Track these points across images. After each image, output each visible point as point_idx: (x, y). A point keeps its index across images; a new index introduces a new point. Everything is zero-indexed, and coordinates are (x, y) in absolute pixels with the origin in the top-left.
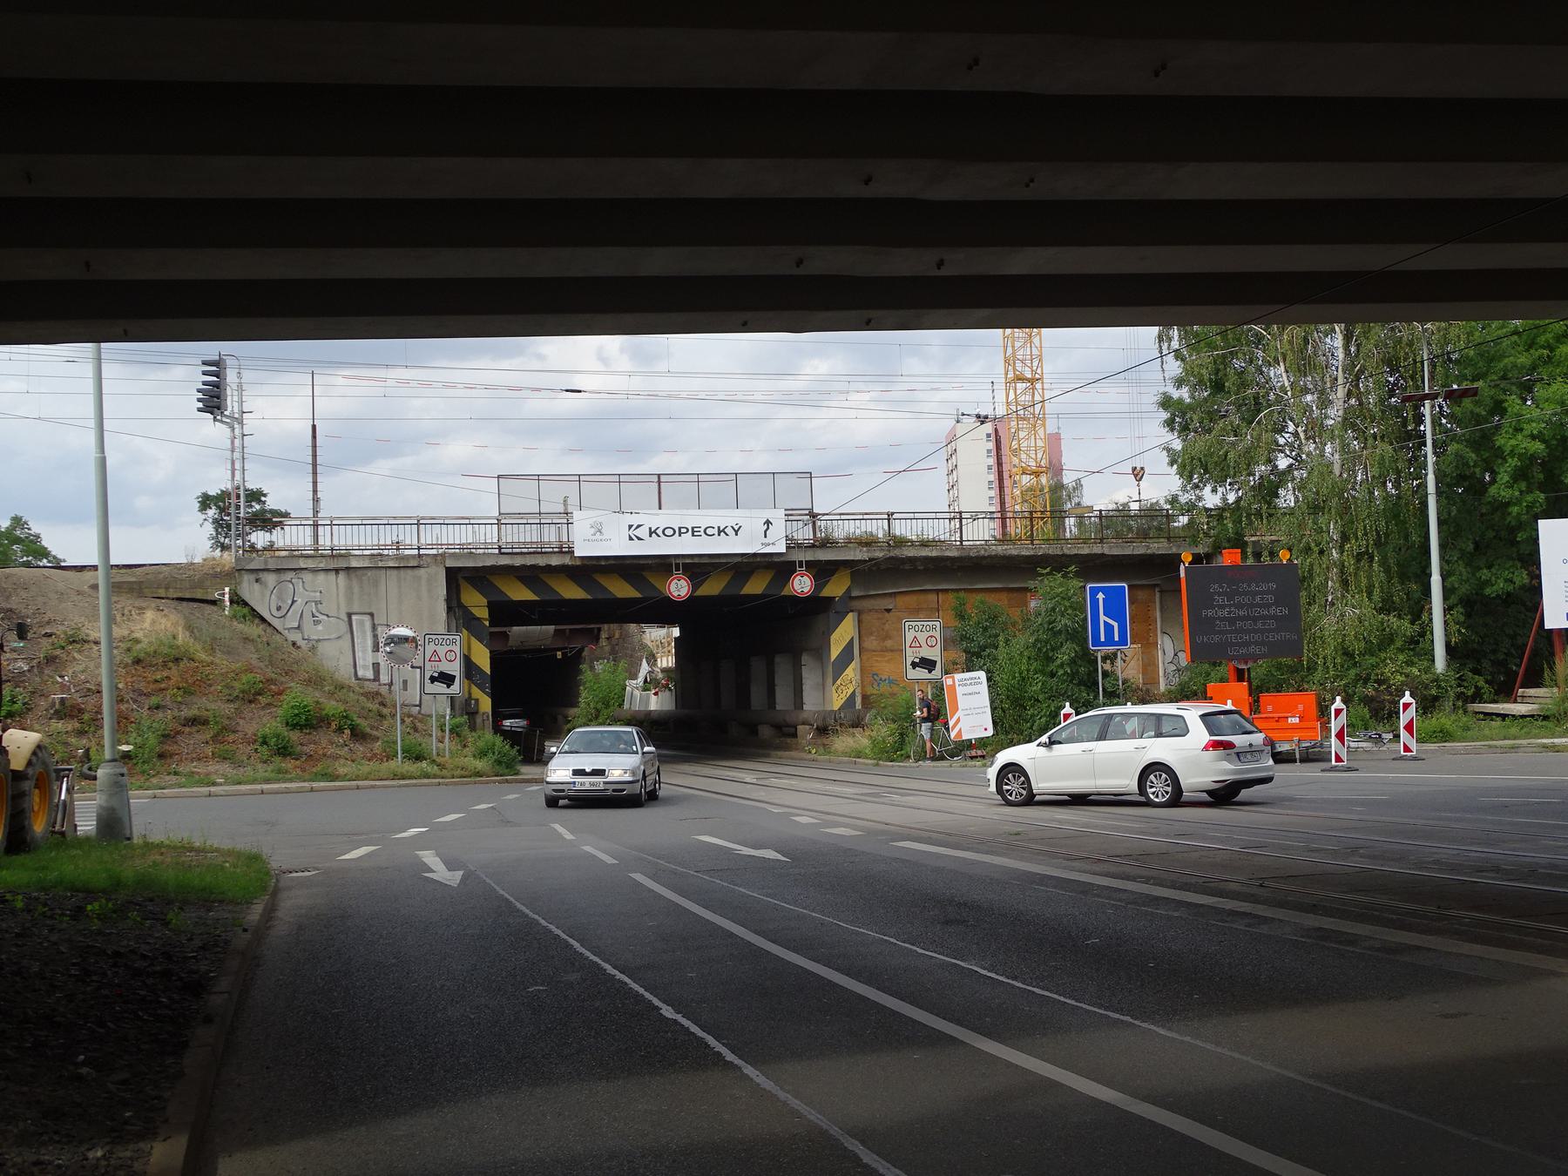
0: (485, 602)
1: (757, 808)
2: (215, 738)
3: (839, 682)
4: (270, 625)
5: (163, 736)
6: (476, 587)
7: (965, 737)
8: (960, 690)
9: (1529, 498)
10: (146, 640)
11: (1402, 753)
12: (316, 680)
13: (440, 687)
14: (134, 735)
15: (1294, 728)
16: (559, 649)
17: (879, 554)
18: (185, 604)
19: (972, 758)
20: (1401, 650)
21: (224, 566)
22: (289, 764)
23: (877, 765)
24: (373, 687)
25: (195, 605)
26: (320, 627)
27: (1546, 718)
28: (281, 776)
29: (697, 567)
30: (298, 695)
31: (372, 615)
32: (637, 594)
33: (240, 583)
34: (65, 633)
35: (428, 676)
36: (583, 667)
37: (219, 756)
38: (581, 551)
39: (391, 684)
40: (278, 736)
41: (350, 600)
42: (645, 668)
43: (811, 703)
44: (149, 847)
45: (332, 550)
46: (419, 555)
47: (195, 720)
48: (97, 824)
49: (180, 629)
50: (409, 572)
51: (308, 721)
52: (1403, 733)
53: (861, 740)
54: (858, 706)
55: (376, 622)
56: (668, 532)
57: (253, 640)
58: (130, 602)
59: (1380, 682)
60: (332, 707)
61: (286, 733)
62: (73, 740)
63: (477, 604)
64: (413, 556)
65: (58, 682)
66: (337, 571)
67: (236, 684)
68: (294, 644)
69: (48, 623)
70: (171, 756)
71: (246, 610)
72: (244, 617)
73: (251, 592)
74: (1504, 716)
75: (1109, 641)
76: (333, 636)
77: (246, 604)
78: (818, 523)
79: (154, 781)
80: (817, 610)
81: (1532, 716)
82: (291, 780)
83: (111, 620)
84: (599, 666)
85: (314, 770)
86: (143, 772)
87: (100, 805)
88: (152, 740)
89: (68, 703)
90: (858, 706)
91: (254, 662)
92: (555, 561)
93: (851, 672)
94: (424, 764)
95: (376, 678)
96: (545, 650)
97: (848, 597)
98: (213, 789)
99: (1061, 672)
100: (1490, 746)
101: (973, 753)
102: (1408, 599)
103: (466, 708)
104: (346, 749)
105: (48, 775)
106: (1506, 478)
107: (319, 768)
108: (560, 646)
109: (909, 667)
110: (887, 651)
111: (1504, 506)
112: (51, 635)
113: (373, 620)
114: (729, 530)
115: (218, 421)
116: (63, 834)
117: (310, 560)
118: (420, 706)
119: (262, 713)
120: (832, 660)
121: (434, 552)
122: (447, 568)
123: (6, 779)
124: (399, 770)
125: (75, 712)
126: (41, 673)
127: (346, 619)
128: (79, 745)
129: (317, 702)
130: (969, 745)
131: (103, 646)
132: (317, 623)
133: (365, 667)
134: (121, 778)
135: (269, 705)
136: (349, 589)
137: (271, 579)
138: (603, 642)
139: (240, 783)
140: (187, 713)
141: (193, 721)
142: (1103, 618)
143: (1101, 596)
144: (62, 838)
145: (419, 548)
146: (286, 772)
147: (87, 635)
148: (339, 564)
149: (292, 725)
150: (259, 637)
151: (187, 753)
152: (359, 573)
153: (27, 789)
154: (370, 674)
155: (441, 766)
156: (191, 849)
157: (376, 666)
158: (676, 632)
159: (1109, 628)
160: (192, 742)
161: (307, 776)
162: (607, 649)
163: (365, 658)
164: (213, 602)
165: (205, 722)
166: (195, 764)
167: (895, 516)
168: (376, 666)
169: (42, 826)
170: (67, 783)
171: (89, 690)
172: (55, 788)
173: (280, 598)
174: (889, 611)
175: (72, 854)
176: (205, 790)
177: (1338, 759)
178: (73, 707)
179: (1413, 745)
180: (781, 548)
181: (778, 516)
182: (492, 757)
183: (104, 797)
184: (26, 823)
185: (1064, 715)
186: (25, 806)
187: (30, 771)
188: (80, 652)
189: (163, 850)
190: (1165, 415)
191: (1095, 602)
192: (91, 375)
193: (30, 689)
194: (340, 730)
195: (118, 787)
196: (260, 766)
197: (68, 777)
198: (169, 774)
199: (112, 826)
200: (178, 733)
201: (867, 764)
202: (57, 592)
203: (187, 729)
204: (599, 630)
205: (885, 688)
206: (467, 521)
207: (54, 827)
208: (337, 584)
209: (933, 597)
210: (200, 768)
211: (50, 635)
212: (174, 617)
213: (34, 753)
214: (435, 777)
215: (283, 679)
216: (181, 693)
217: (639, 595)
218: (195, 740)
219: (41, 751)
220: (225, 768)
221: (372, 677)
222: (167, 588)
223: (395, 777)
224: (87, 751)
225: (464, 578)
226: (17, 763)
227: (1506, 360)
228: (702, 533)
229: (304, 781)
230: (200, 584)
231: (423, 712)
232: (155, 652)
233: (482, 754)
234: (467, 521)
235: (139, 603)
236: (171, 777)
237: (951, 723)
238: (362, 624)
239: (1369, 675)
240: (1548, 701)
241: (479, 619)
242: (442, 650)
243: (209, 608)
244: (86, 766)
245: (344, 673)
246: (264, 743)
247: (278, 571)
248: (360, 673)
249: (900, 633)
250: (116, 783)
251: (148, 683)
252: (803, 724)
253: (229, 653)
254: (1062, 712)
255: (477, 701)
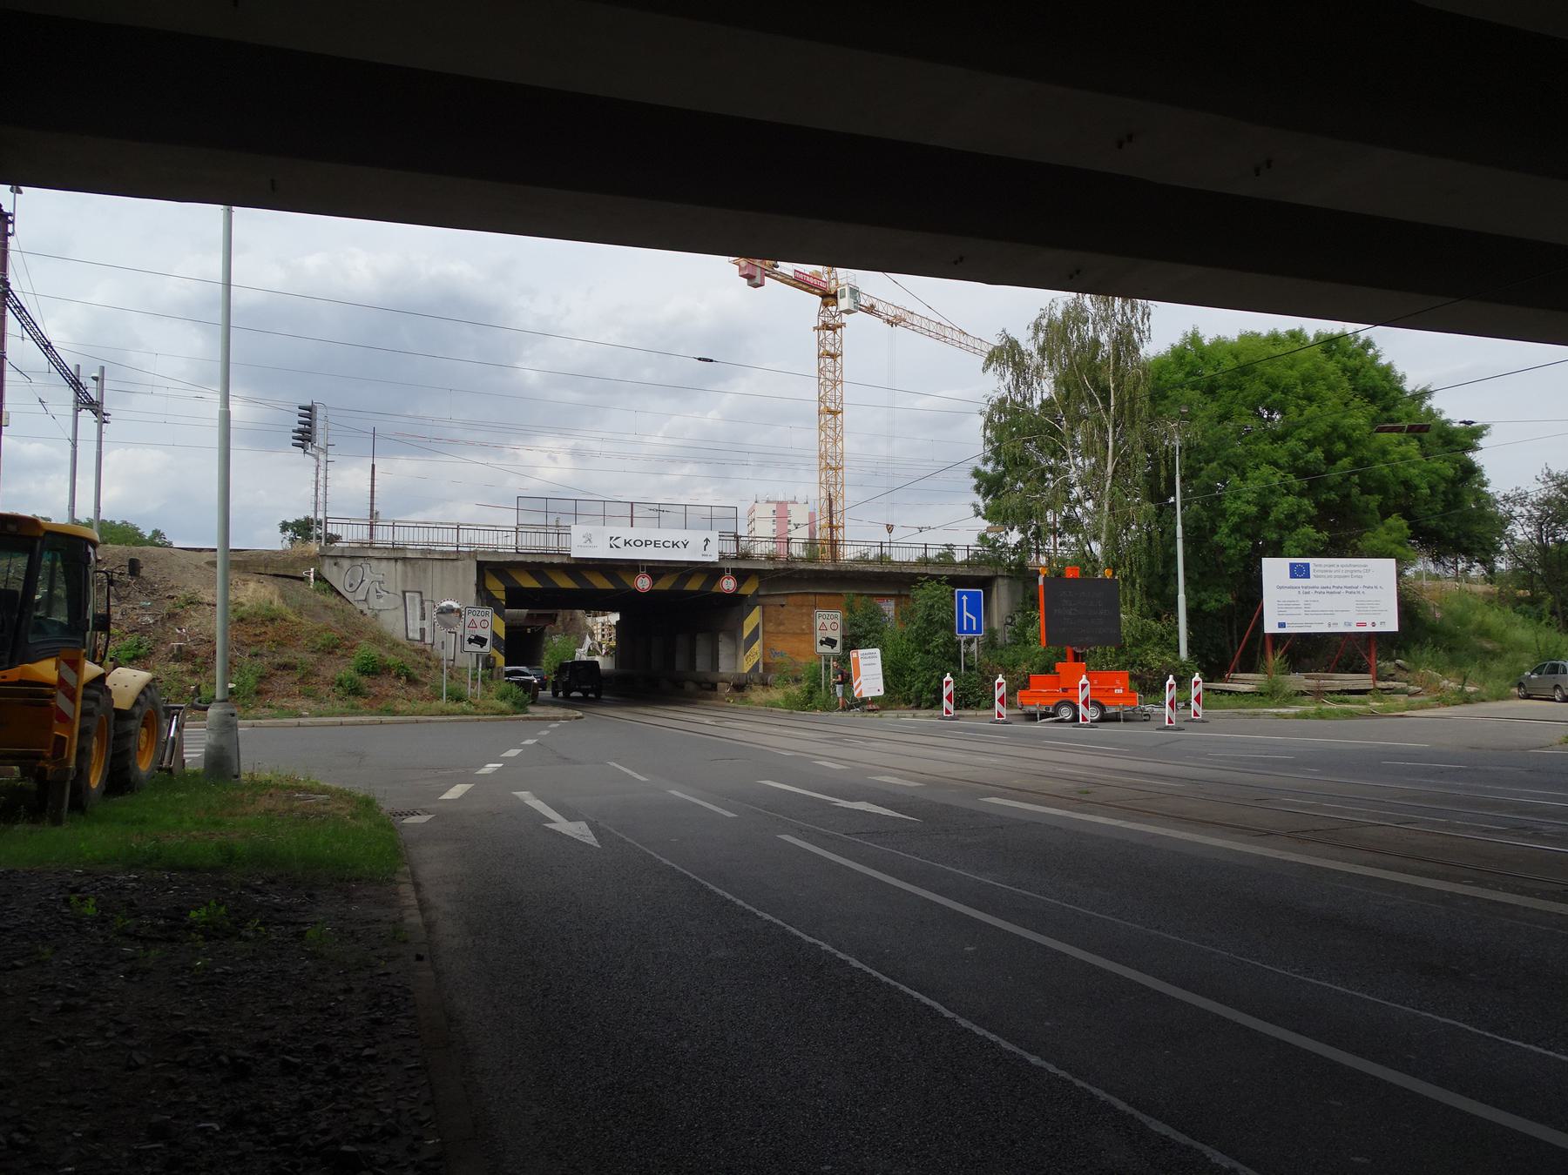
0: (503, 587)
1: (742, 746)
2: (301, 680)
3: (748, 654)
4: (344, 597)
5: (260, 677)
6: (497, 576)
7: (864, 695)
8: (861, 662)
9: (1241, 544)
10: (249, 605)
11: (1193, 717)
12: (379, 639)
13: (476, 647)
14: (237, 676)
15: (1118, 697)
16: (529, 627)
17: (781, 566)
18: (280, 579)
19: (869, 710)
20: (1156, 645)
21: (311, 552)
22: (360, 701)
23: (791, 713)
24: (419, 645)
25: (288, 580)
26: (381, 601)
27: (1261, 694)
28: (355, 710)
29: (656, 569)
30: (365, 649)
31: (421, 593)
32: (611, 587)
33: (323, 565)
34: (185, 596)
35: (466, 639)
36: (546, 639)
37: (305, 694)
38: (578, 552)
39: (432, 645)
40: (351, 680)
41: (405, 581)
42: (588, 641)
43: (725, 666)
44: (260, 788)
45: (393, 544)
46: (458, 551)
47: (285, 665)
48: (205, 752)
49: (276, 597)
50: (450, 563)
51: (374, 669)
52: (1193, 703)
53: (776, 695)
54: (761, 671)
55: (424, 598)
56: (638, 543)
57: (331, 608)
58: (237, 575)
59: (1142, 665)
60: (391, 659)
61: (358, 678)
62: (187, 679)
63: (497, 589)
64: (454, 552)
65: (177, 633)
66: (396, 560)
67: (319, 640)
68: (362, 612)
69: (172, 588)
70: (267, 692)
71: (326, 586)
72: (325, 590)
73: (330, 572)
74: (1230, 692)
75: (970, 630)
76: (392, 607)
77: (326, 581)
78: (740, 543)
79: (252, 712)
80: (737, 605)
81: (1253, 693)
82: (362, 714)
83: (227, 586)
84: (556, 639)
85: (379, 706)
86: (243, 705)
87: (209, 745)
88: (252, 680)
89: (184, 649)
90: (761, 671)
91: (332, 624)
92: (556, 560)
93: (757, 647)
94: (464, 704)
95: (422, 639)
96: (520, 627)
97: (756, 595)
98: (302, 720)
99: (936, 651)
100: (1239, 713)
101: (870, 707)
102: (1151, 610)
103: (488, 663)
104: (403, 691)
105: (156, 712)
106: (1227, 530)
107: (383, 705)
108: (530, 624)
109: (818, 644)
110: (780, 633)
111: (1222, 549)
112: (173, 598)
113: (421, 597)
114: (680, 544)
115: (307, 453)
116: (170, 771)
117: (376, 551)
118: (454, 660)
119: (338, 662)
120: (745, 638)
121: (467, 549)
122: (478, 561)
123: (107, 720)
124: (446, 708)
125: (190, 657)
126: (164, 625)
127: (401, 595)
128: (192, 683)
129: (380, 655)
130: (864, 701)
131: (219, 608)
132: (379, 597)
133: (414, 631)
134: (230, 717)
135: (344, 656)
136: (405, 573)
137: (346, 563)
138: (559, 623)
139: (321, 716)
140: (278, 660)
141: (285, 667)
142: (966, 614)
143: (965, 598)
144: (170, 775)
145: (458, 546)
146: (358, 708)
147: (202, 598)
148: (397, 555)
149: (362, 672)
150: (336, 605)
151: (279, 691)
152: (413, 562)
153: (133, 728)
154: (418, 637)
155: (477, 706)
156: (300, 789)
157: (422, 631)
158: (614, 618)
159: (970, 621)
160: (283, 682)
161: (374, 711)
162: (561, 627)
163: (415, 624)
164: (302, 579)
165: (294, 668)
166: (285, 699)
167: (792, 541)
168: (422, 631)
169: (148, 765)
170: (177, 721)
171: (202, 640)
172: (165, 725)
173: (352, 577)
174: (783, 606)
175: (177, 797)
176: (295, 721)
177: (1170, 721)
178: (188, 652)
179: (1200, 712)
180: (715, 558)
181: (714, 536)
182: (510, 700)
183: (213, 736)
184: (130, 763)
185: (1195, 682)
186: (131, 745)
187: (137, 710)
188: (195, 611)
189: (272, 790)
190: (975, 481)
191: (961, 602)
192: (216, 444)
193: (154, 637)
194: (398, 676)
195: (227, 726)
196: (337, 702)
197: (178, 716)
198: (265, 707)
199: (220, 764)
200: (272, 675)
201: (783, 712)
202: (179, 566)
203: (280, 673)
204: (557, 615)
205: (778, 659)
206: (495, 528)
207: (162, 764)
208: (396, 570)
209: (812, 598)
210: (289, 703)
211: (173, 598)
212: (271, 588)
213: (143, 692)
214: (472, 714)
215: (354, 637)
216: (274, 644)
217: (613, 587)
218: (284, 681)
219: (151, 690)
220: (310, 703)
221: (419, 639)
222: (266, 567)
223: (443, 713)
224: (198, 687)
225: (488, 569)
226: (123, 701)
227: (1230, 450)
228: (661, 545)
229: (372, 715)
230: (292, 564)
231: (456, 665)
232: (255, 613)
233: (503, 697)
234: (494, 528)
235: (244, 577)
236: (266, 709)
237: (855, 685)
238: (413, 601)
239: (1135, 662)
240: (1263, 683)
241: (498, 599)
242: (478, 620)
243: (298, 583)
244: (197, 699)
245: (399, 635)
246: (340, 684)
247: (351, 558)
248: (411, 635)
249: (812, 620)
250: (227, 722)
251: (249, 636)
252: (722, 682)
253: (313, 616)
254: (996, 682)
255: (495, 658)
